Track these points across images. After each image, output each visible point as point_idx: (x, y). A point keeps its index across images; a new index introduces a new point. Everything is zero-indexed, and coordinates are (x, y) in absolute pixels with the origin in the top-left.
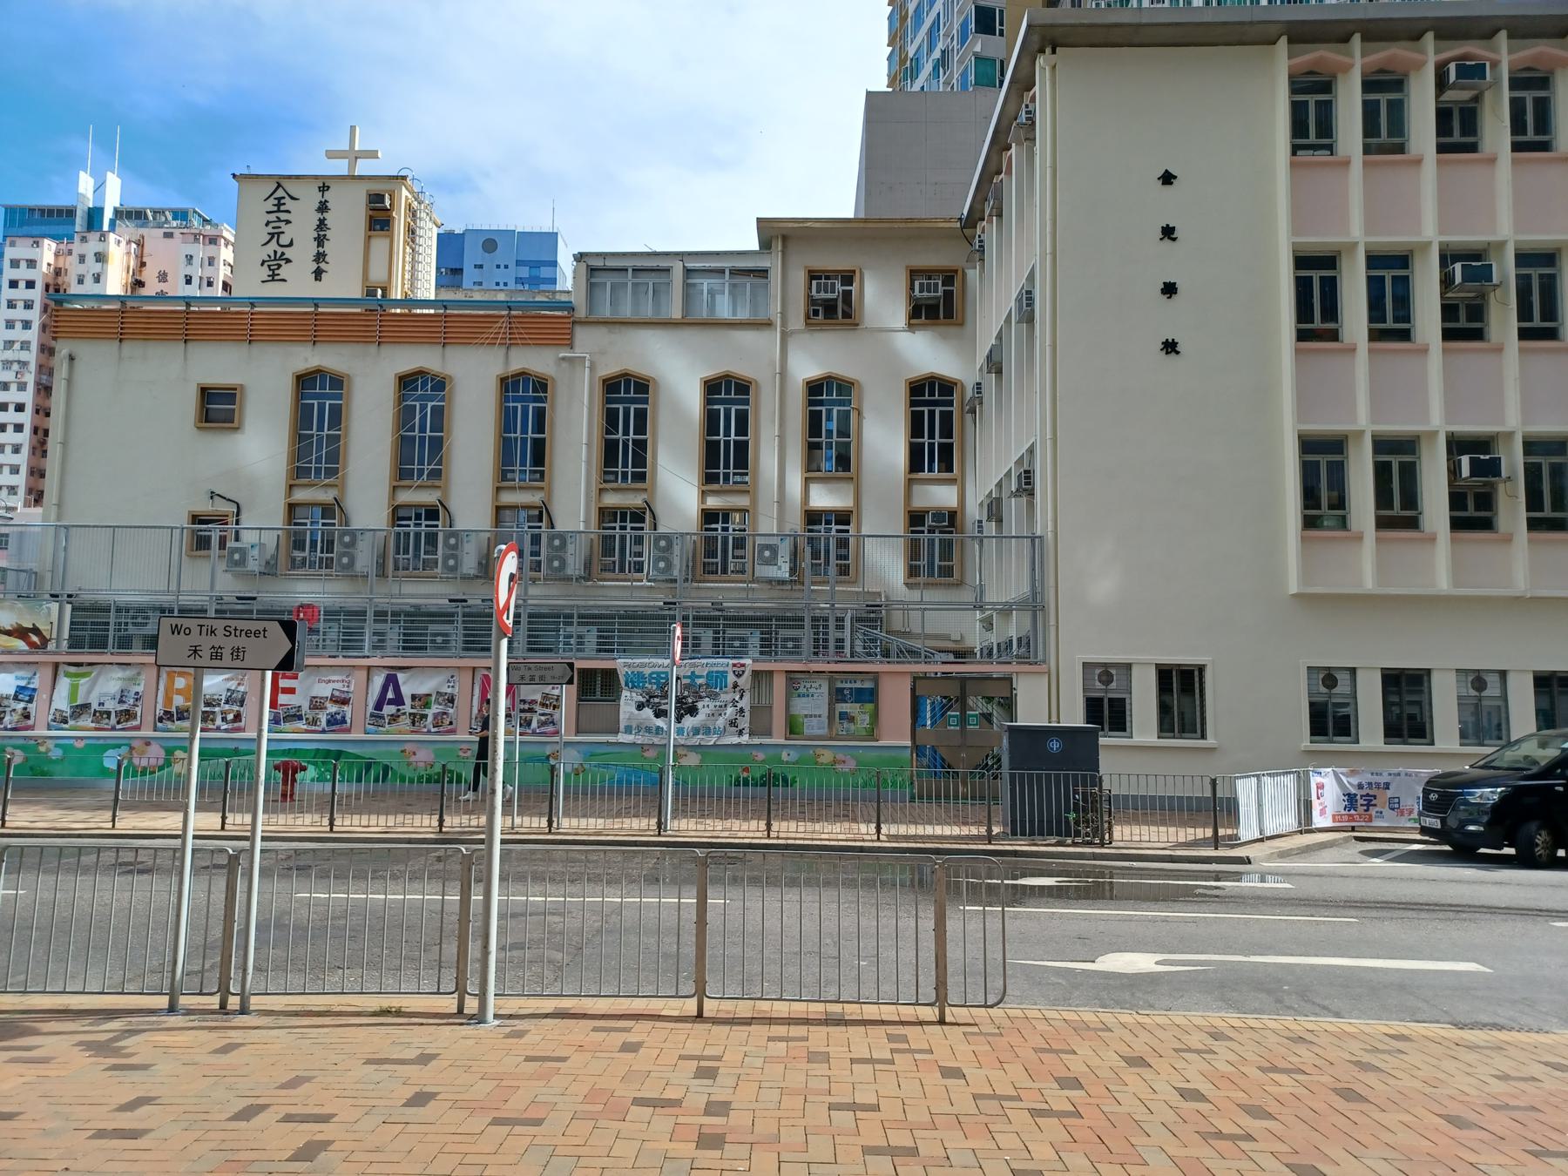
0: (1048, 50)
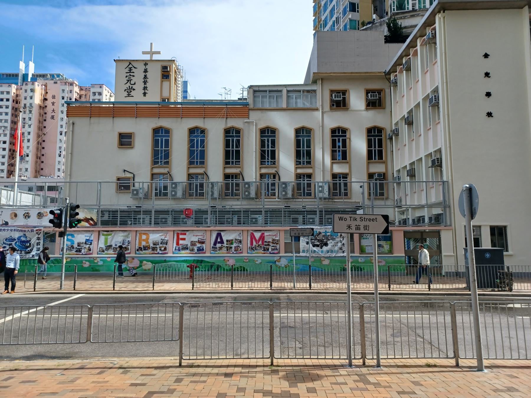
0: (442, 12)
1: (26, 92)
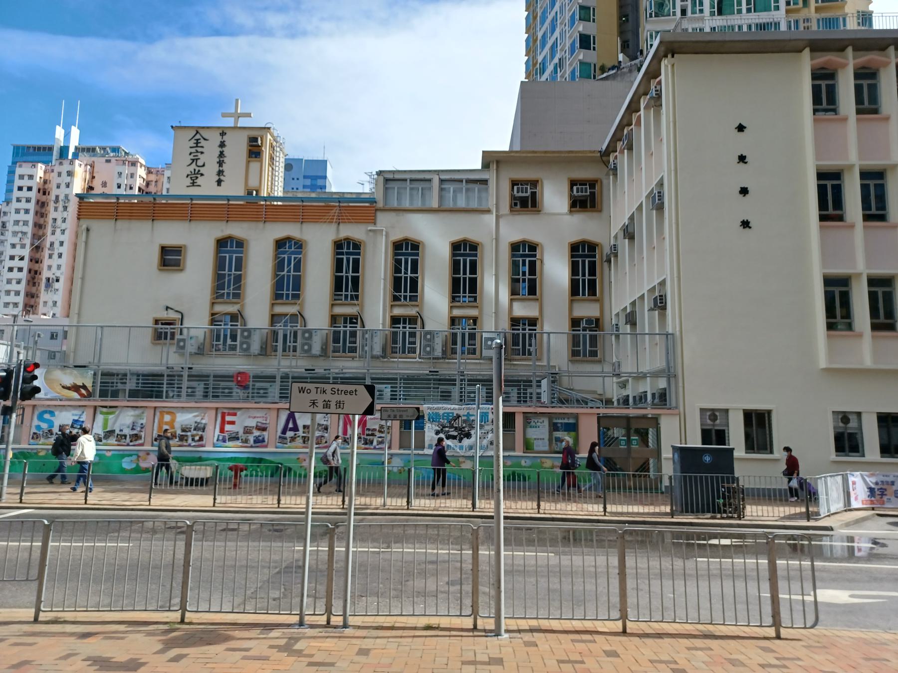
0: (670, 56)
1: (60, 176)
